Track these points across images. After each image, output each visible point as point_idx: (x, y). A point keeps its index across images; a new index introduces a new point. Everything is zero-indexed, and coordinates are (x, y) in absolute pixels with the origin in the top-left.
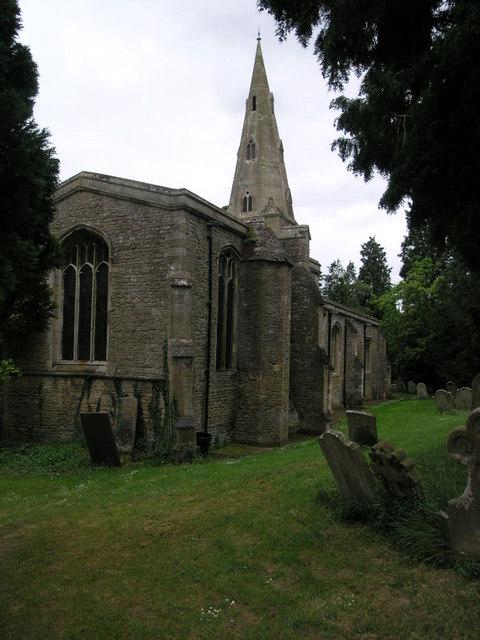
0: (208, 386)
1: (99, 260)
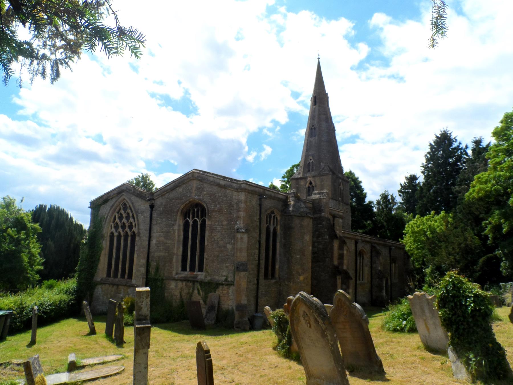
0: (258, 288)
1: (202, 217)
